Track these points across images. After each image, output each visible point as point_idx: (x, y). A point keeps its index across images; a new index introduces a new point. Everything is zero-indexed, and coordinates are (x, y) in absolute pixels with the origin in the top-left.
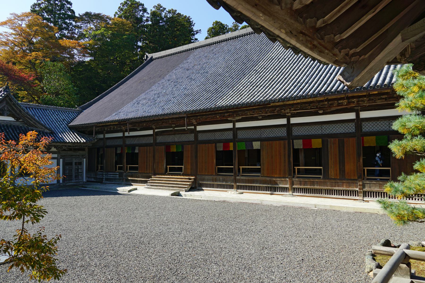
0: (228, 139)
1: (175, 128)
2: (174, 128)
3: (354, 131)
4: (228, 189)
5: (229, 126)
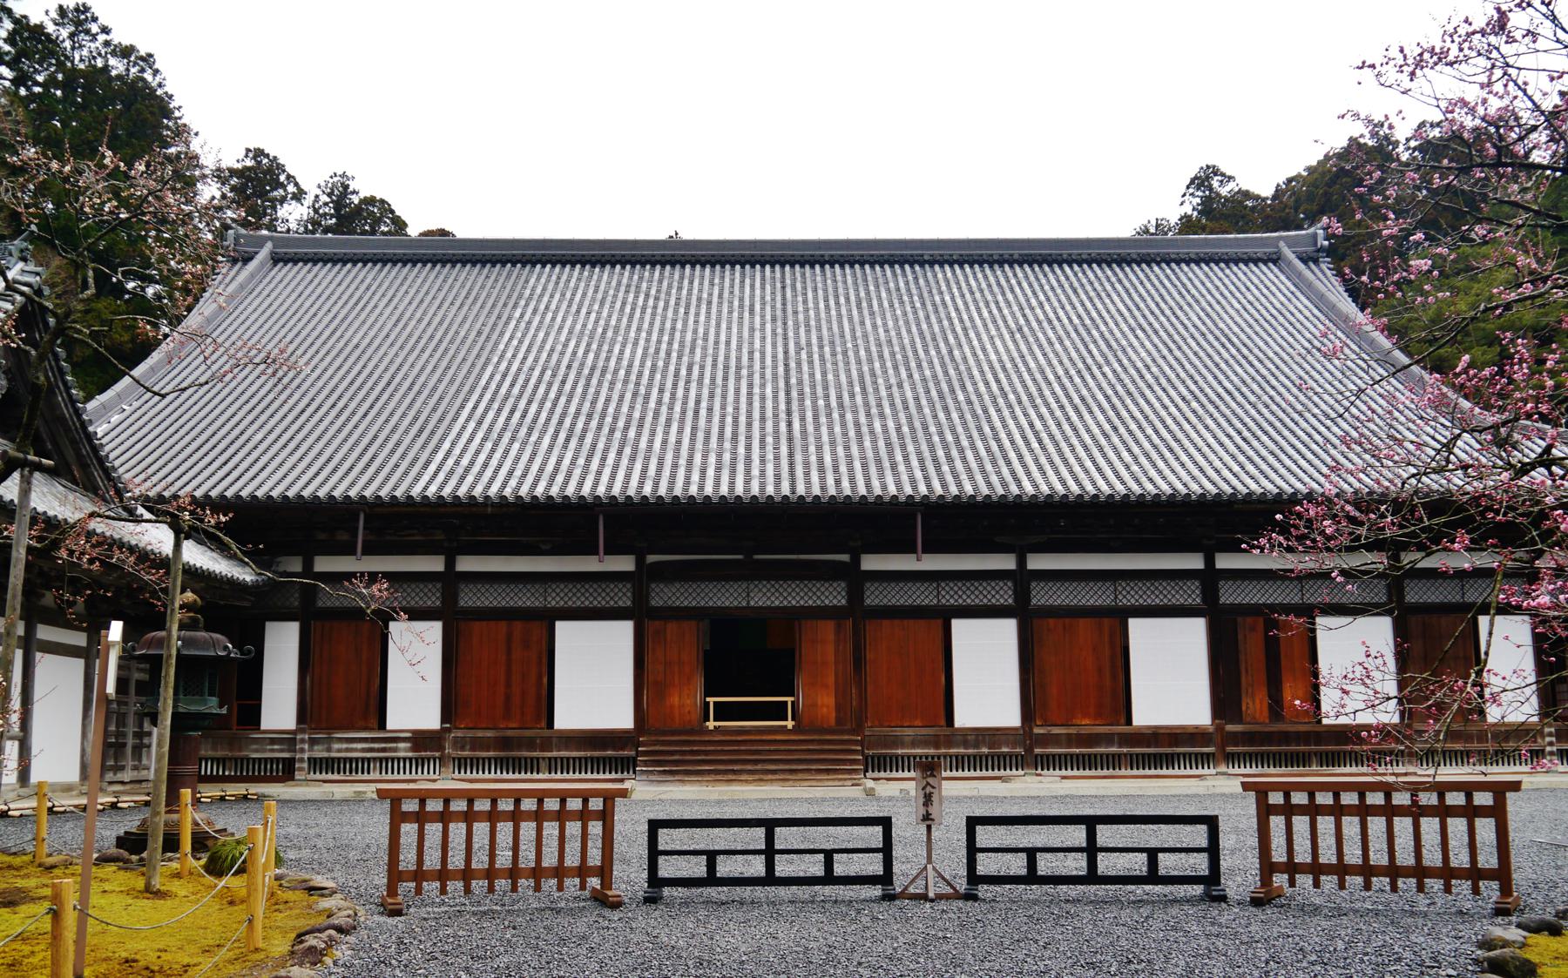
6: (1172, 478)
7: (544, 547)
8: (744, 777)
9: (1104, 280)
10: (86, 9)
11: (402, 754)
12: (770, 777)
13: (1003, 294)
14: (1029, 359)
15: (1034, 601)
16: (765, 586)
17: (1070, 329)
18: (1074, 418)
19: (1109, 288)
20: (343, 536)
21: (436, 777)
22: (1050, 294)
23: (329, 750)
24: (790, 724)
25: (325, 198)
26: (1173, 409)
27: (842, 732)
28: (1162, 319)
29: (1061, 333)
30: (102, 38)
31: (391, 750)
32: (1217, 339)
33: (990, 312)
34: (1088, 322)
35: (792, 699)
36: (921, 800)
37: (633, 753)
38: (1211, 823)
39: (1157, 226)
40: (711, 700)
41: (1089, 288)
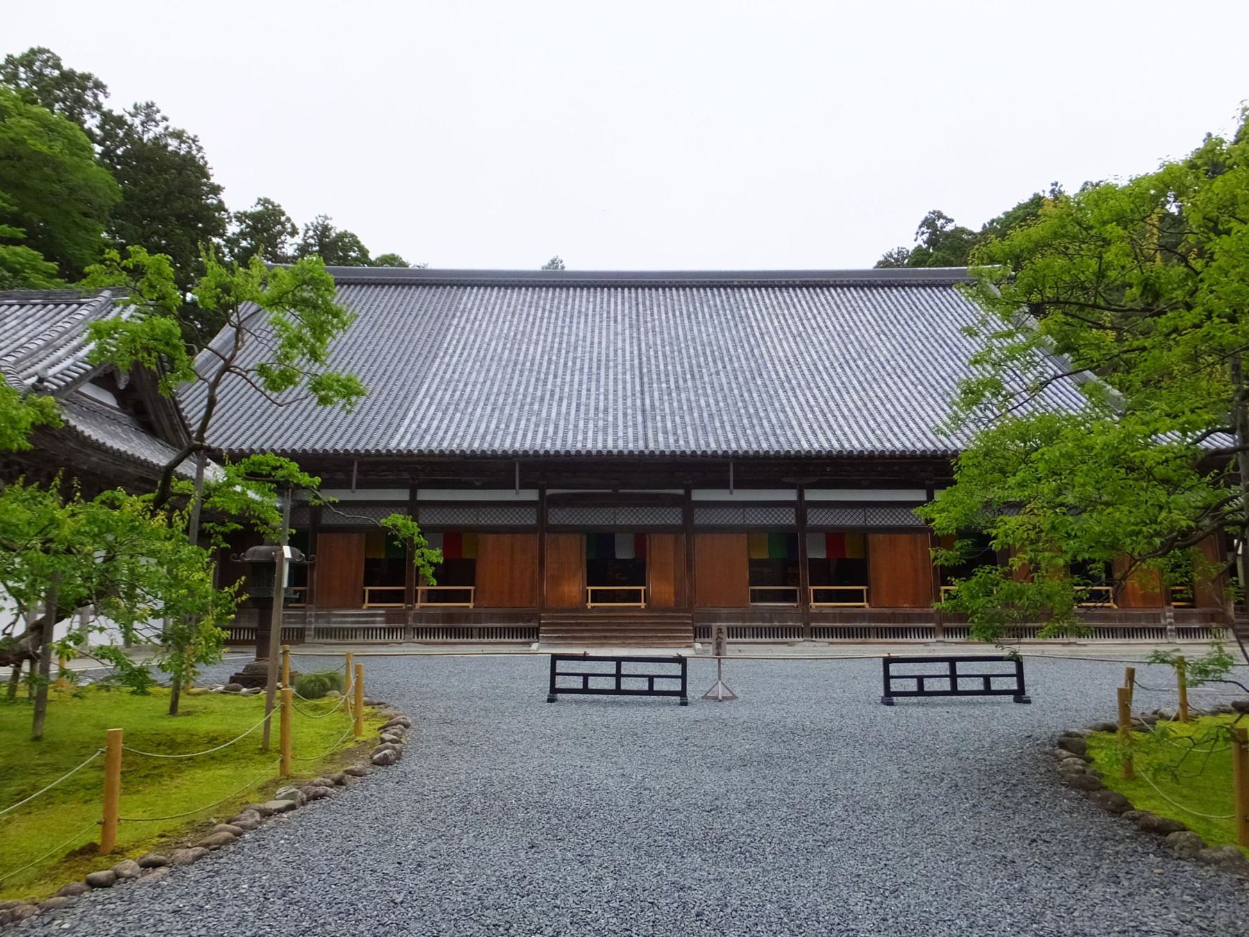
1: (620, 491)
4: (797, 639)
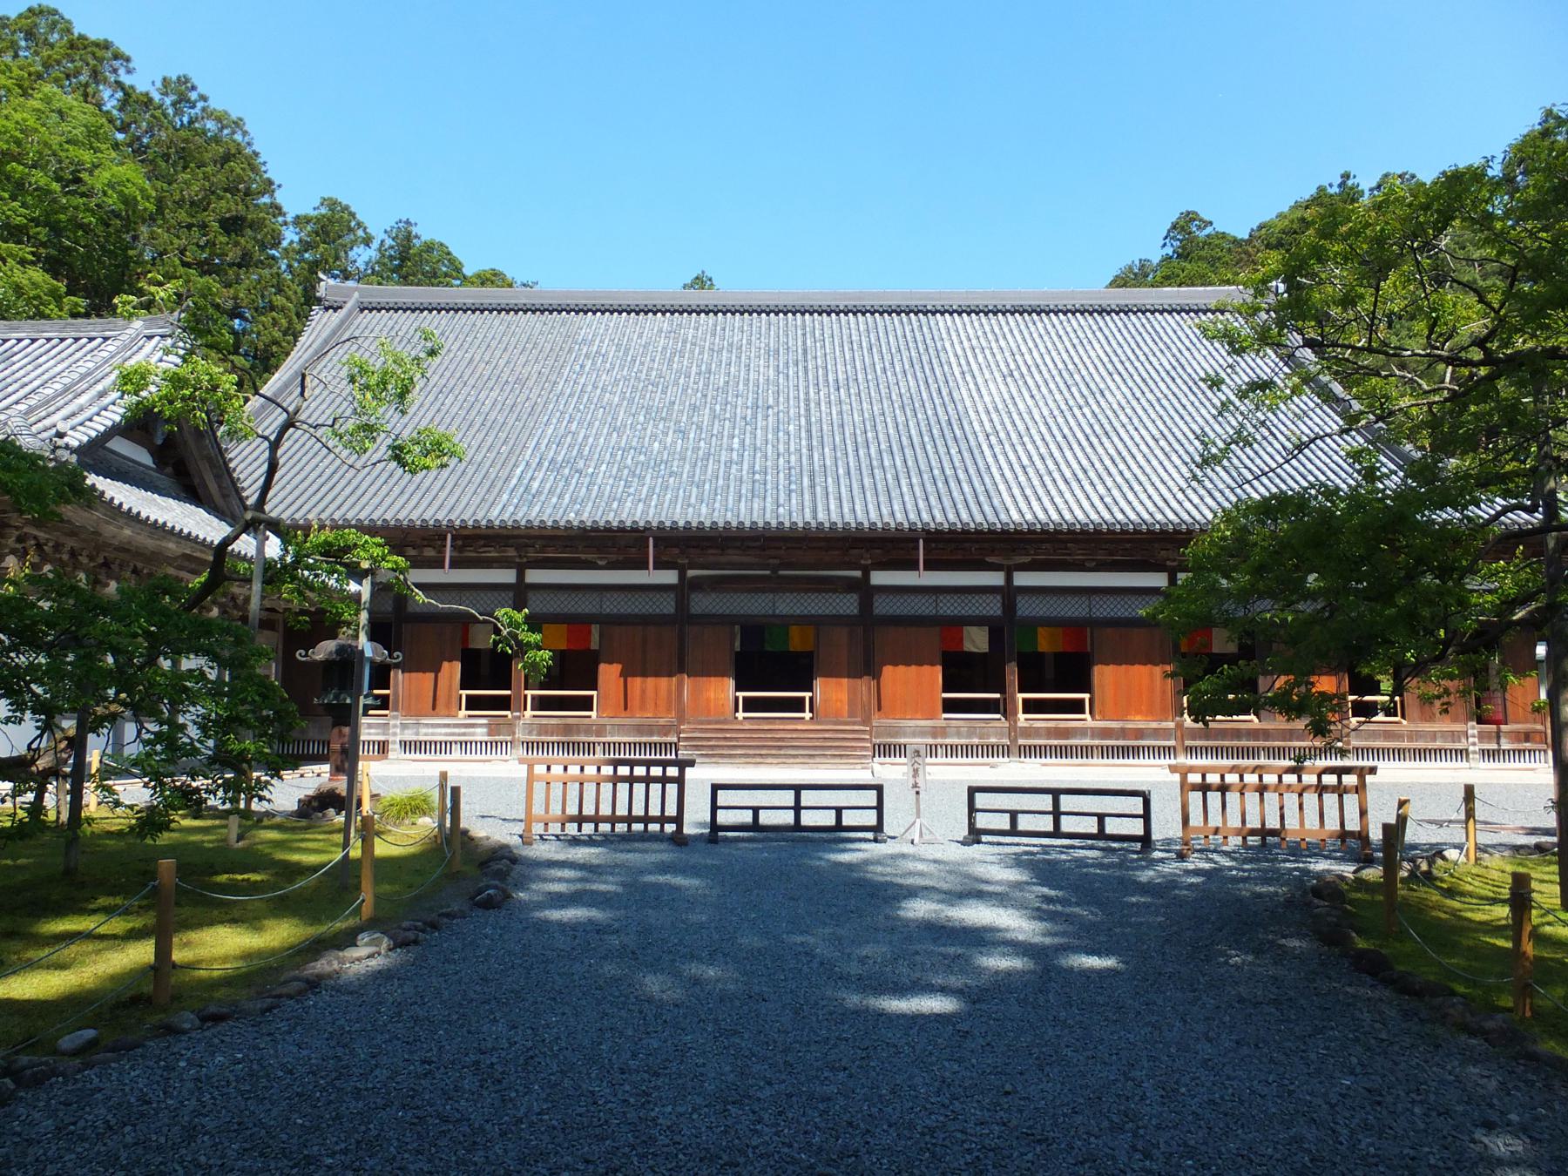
0: (664, 615)
1: (781, 572)
2: (775, 569)
3: (672, 611)
5: (995, 579)
6: (1139, 508)
7: (600, 563)
8: (770, 760)
9: (1086, 329)
10: (187, 80)
11: (479, 738)
12: (792, 760)
13: (997, 341)
14: (1018, 400)
15: (1019, 613)
16: (788, 597)
17: (1055, 372)
18: (1057, 454)
19: (1090, 336)
20: (429, 553)
21: (508, 757)
22: (1038, 340)
23: (417, 734)
24: (807, 715)
25: (389, 242)
26: (1143, 447)
27: (854, 723)
28: (1137, 364)
29: (1047, 376)
30: (200, 105)
31: (470, 734)
32: (1185, 382)
33: (985, 357)
34: (1071, 367)
35: (810, 694)
36: (912, 773)
37: (675, 739)
38: (1146, 798)
39: (1142, 266)
40: (741, 695)
41: (1072, 335)
